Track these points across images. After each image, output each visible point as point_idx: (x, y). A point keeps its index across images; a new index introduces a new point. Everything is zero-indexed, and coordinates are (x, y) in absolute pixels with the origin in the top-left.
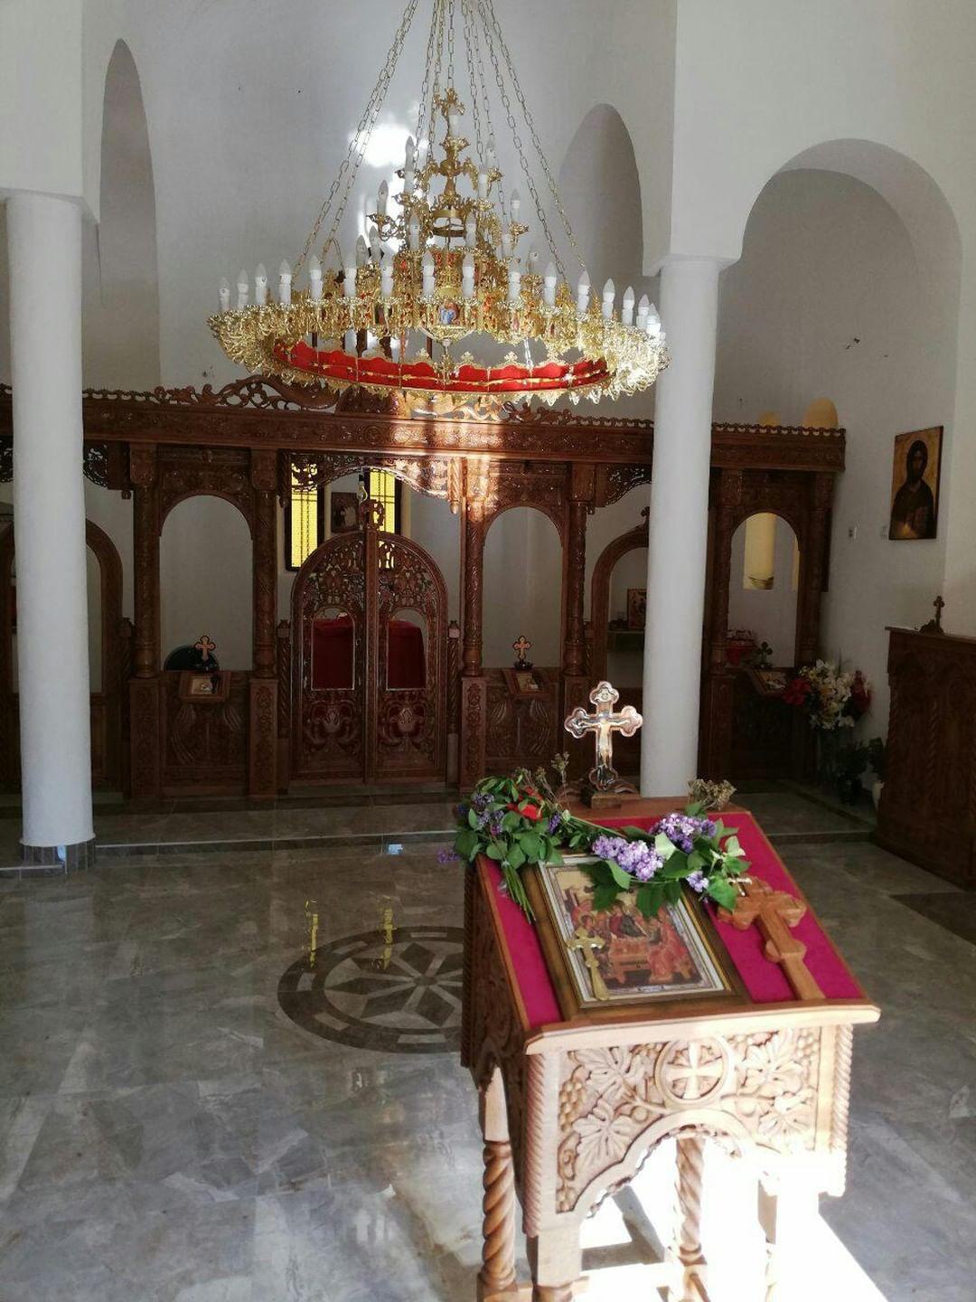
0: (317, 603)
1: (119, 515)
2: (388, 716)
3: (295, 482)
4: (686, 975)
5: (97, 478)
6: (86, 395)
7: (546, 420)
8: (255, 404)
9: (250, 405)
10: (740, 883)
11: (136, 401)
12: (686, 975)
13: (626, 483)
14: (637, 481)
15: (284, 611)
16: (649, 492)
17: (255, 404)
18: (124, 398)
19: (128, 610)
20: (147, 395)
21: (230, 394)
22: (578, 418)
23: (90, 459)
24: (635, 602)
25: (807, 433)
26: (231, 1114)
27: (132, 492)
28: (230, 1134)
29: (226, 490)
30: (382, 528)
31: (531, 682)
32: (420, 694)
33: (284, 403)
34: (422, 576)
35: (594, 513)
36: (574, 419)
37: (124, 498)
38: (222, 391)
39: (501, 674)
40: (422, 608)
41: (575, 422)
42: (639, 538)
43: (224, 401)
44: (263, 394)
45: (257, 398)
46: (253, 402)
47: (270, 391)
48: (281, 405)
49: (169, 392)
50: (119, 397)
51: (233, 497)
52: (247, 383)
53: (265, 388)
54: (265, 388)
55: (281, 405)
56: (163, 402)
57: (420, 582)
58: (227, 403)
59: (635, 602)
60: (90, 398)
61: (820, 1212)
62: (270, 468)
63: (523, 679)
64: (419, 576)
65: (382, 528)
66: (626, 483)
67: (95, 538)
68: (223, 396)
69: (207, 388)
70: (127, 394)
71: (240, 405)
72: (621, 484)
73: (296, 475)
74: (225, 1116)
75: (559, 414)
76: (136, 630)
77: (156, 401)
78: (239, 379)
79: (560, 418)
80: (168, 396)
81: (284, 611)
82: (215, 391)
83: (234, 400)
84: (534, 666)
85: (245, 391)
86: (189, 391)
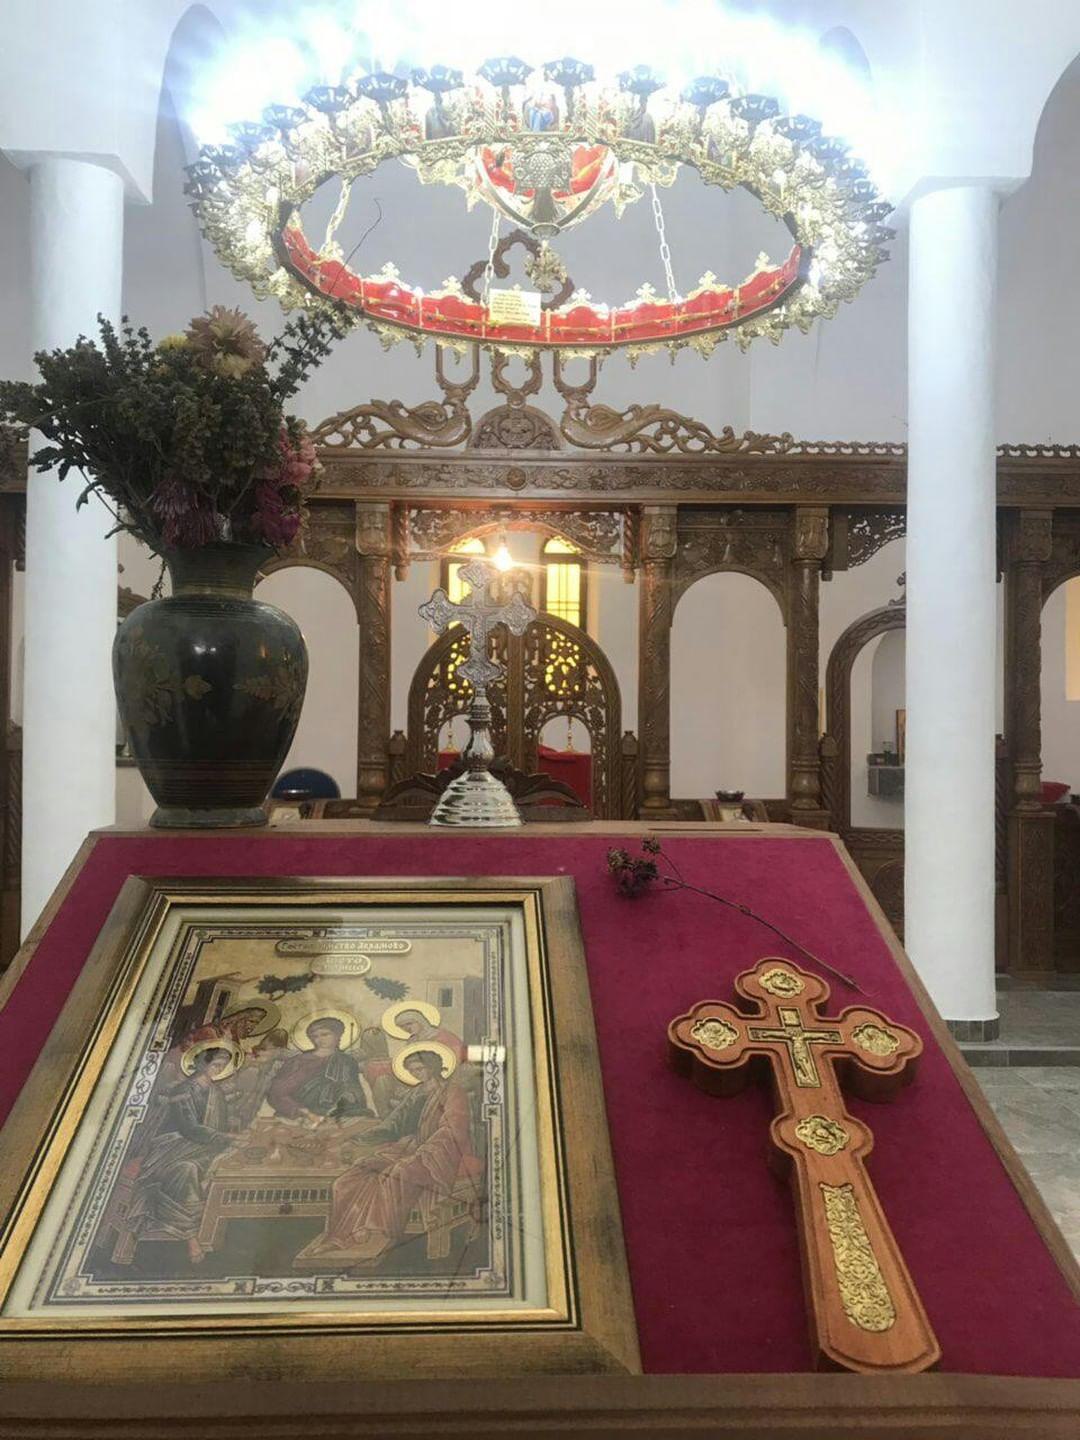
4: (438, 1247)
5: (861, 556)
6: (1001, 453)
8: (360, 442)
9: (355, 445)
12: (438, 1247)
13: (877, 537)
16: (903, 548)
17: (360, 442)
22: (804, 445)
25: (1034, 453)
33: (399, 441)
36: (797, 446)
38: (321, 426)
40: (585, 715)
41: (799, 450)
42: (892, 619)
44: (371, 429)
45: (365, 436)
46: (358, 441)
47: (381, 426)
48: (395, 443)
50: (839, 450)
52: (350, 417)
53: (375, 421)
54: (375, 421)
55: (395, 443)
58: (326, 444)
60: (1006, 454)
66: (877, 537)
71: (345, 444)
72: (871, 538)
75: (776, 439)
78: (341, 411)
81: (399, 721)
83: (335, 439)
84: (745, 797)
85: (348, 427)
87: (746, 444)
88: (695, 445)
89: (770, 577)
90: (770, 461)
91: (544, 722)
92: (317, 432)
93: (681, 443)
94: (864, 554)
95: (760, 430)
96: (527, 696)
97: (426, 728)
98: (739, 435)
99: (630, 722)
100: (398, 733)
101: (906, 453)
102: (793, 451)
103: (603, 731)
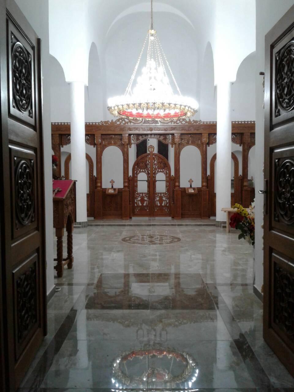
1: (93, 151)
7: (195, 123)
9: (122, 124)
10: (279, 109)
18: (249, 122)
19: (95, 174)
20: (99, 123)
21: (117, 122)
22: (204, 122)
27: (96, 146)
29: (117, 144)
30: (153, 152)
35: (209, 146)
37: (94, 147)
38: (116, 120)
43: (116, 123)
45: (124, 122)
49: (104, 122)
51: (119, 146)
56: (102, 124)
61: (266, 36)
65: (153, 152)
67: (88, 157)
68: (116, 122)
69: (112, 121)
71: (120, 124)
75: (198, 121)
76: (96, 178)
79: (199, 122)
80: (103, 123)
81: (130, 174)
83: (118, 123)
85: (121, 121)
86: (108, 121)
87: (193, 122)
88: (184, 122)
89: (198, 146)
91: (139, 173)
92: (115, 122)
93: (181, 122)
94: (234, 142)
95: (195, 120)
96: (154, 169)
97: (135, 175)
98: (192, 120)
100: (131, 176)
101: (216, 123)
102: (202, 123)
103: (168, 175)
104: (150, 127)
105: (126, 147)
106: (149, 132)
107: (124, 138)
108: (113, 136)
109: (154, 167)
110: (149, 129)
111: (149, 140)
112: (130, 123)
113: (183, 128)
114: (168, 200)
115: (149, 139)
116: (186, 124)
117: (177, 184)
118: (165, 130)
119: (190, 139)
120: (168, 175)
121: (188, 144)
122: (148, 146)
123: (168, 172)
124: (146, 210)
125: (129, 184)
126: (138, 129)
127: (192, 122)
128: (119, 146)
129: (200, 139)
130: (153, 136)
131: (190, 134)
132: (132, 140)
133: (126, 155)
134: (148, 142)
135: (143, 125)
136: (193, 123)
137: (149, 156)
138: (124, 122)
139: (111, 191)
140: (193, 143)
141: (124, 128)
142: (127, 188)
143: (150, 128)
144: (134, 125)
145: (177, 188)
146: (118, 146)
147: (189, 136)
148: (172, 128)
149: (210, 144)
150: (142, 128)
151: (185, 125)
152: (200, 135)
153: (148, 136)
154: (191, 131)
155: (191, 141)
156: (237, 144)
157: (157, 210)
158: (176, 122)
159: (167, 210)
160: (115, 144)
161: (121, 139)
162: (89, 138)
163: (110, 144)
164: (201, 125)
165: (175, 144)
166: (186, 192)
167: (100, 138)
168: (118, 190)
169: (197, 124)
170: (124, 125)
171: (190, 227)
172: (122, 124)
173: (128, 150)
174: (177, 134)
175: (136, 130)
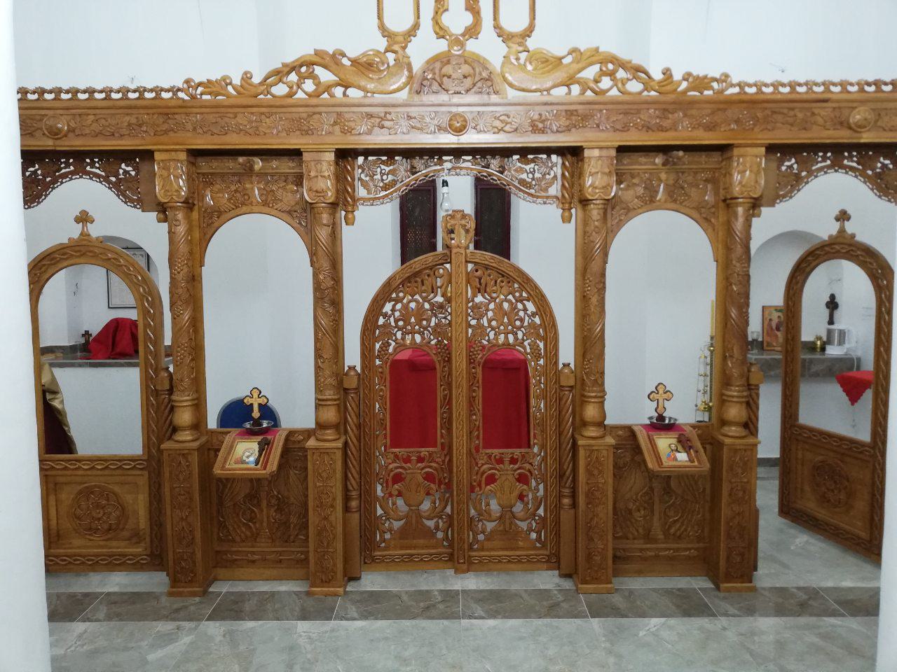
0: (393, 344)
2: (483, 485)
3: (362, 192)
9: (300, 95)
11: (162, 99)
14: (821, 169)
15: (352, 356)
23: (122, 176)
24: (771, 320)
26: (313, 646)
28: (309, 660)
29: (279, 206)
31: (677, 450)
32: (523, 456)
34: (524, 305)
39: (630, 432)
47: (325, 75)
48: (338, 91)
49: (200, 84)
52: (293, 68)
53: (319, 71)
54: (319, 71)
56: (193, 97)
57: (521, 313)
59: (771, 320)
62: (326, 174)
63: (665, 443)
64: (520, 306)
69: (247, 77)
70: (168, 91)
71: (291, 95)
73: (365, 184)
74: (308, 646)
77: (186, 98)
81: (352, 356)
82: (256, 79)
83: (280, 90)
86: (226, 81)
87: (684, 85)
88: (634, 86)
89: (704, 216)
90: (709, 101)
92: (261, 84)
95: (698, 71)
98: (677, 76)
99: (567, 353)
103: (542, 362)
104: (454, 109)
105: (325, 218)
106: (447, 140)
107: (313, 174)
108: (258, 164)
109: (473, 322)
110: (446, 119)
111: (445, 183)
112: (346, 87)
113: (628, 109)
114: (541, 487)
115: (445, 178)
116: (645, 93)
117: (590, 412)
118: (535, 129)
119: (663, 176)
120: (542, 362)
121: (649, 202)
122: (443, 214)
123: (541, 345)
124: (433, 535)
125: (342, 408)
126: (387, 124)
127: (679, 83)
128: (289, 213)
129: (718, 179)
130: (468, 165)
131: (665, 149)
132: (357, 183)
133: (326, 265)
134: (442, 191)
135: (417, 99)
136: (685, 92)
137: (448, 266)
138: (309, 86)
139: (488, 157)
140: (677, 200)
141: (310, 115)
142: (330, 434)
143: (454, 116)
144: (367, 101)
145: (592, 432)
146: (285, 216)
147: (659, 160)
148: (570, 113)
149: (762, 205)
150: (410, 118)
151: (646, 102)
152: (716, 157)
153: (441, 162)
154: (671, 134)
155: (666, 185)
156: (761, 211)
157: (488, 539)
158: (592, 85)
159: (539, 533)
160: (268, 204)
161: (299, 180)
162: (133, 173)
163: (241, 205)
164: (731, 102)
165: (584, 202)
166: (646, 466)
167: (182, 169)
168: (287, 439)
169: (708, 93)
170: (314, 101)
171: (312, 104)
172: (300, 95)
173: (335, 236)
174: (601, 148)
175: (376, 129)
